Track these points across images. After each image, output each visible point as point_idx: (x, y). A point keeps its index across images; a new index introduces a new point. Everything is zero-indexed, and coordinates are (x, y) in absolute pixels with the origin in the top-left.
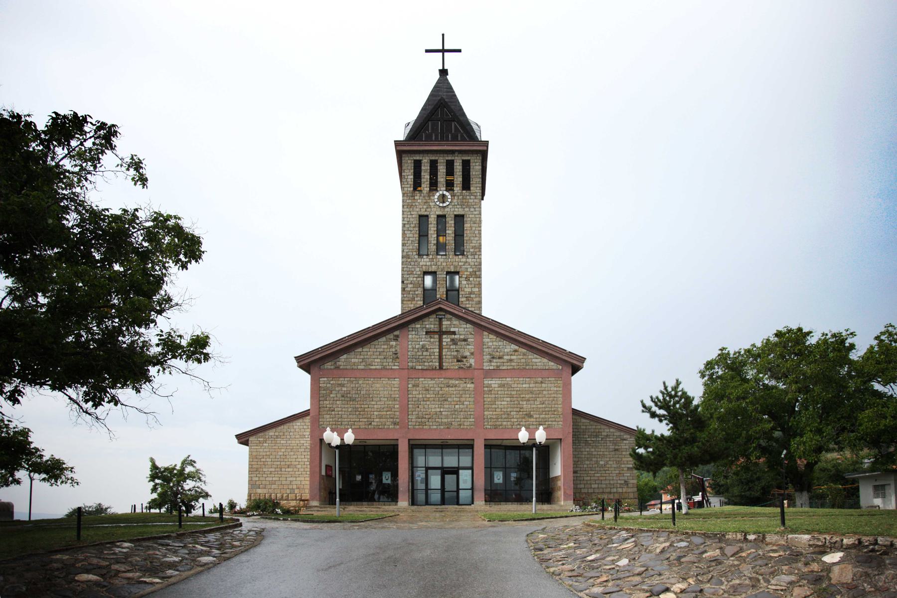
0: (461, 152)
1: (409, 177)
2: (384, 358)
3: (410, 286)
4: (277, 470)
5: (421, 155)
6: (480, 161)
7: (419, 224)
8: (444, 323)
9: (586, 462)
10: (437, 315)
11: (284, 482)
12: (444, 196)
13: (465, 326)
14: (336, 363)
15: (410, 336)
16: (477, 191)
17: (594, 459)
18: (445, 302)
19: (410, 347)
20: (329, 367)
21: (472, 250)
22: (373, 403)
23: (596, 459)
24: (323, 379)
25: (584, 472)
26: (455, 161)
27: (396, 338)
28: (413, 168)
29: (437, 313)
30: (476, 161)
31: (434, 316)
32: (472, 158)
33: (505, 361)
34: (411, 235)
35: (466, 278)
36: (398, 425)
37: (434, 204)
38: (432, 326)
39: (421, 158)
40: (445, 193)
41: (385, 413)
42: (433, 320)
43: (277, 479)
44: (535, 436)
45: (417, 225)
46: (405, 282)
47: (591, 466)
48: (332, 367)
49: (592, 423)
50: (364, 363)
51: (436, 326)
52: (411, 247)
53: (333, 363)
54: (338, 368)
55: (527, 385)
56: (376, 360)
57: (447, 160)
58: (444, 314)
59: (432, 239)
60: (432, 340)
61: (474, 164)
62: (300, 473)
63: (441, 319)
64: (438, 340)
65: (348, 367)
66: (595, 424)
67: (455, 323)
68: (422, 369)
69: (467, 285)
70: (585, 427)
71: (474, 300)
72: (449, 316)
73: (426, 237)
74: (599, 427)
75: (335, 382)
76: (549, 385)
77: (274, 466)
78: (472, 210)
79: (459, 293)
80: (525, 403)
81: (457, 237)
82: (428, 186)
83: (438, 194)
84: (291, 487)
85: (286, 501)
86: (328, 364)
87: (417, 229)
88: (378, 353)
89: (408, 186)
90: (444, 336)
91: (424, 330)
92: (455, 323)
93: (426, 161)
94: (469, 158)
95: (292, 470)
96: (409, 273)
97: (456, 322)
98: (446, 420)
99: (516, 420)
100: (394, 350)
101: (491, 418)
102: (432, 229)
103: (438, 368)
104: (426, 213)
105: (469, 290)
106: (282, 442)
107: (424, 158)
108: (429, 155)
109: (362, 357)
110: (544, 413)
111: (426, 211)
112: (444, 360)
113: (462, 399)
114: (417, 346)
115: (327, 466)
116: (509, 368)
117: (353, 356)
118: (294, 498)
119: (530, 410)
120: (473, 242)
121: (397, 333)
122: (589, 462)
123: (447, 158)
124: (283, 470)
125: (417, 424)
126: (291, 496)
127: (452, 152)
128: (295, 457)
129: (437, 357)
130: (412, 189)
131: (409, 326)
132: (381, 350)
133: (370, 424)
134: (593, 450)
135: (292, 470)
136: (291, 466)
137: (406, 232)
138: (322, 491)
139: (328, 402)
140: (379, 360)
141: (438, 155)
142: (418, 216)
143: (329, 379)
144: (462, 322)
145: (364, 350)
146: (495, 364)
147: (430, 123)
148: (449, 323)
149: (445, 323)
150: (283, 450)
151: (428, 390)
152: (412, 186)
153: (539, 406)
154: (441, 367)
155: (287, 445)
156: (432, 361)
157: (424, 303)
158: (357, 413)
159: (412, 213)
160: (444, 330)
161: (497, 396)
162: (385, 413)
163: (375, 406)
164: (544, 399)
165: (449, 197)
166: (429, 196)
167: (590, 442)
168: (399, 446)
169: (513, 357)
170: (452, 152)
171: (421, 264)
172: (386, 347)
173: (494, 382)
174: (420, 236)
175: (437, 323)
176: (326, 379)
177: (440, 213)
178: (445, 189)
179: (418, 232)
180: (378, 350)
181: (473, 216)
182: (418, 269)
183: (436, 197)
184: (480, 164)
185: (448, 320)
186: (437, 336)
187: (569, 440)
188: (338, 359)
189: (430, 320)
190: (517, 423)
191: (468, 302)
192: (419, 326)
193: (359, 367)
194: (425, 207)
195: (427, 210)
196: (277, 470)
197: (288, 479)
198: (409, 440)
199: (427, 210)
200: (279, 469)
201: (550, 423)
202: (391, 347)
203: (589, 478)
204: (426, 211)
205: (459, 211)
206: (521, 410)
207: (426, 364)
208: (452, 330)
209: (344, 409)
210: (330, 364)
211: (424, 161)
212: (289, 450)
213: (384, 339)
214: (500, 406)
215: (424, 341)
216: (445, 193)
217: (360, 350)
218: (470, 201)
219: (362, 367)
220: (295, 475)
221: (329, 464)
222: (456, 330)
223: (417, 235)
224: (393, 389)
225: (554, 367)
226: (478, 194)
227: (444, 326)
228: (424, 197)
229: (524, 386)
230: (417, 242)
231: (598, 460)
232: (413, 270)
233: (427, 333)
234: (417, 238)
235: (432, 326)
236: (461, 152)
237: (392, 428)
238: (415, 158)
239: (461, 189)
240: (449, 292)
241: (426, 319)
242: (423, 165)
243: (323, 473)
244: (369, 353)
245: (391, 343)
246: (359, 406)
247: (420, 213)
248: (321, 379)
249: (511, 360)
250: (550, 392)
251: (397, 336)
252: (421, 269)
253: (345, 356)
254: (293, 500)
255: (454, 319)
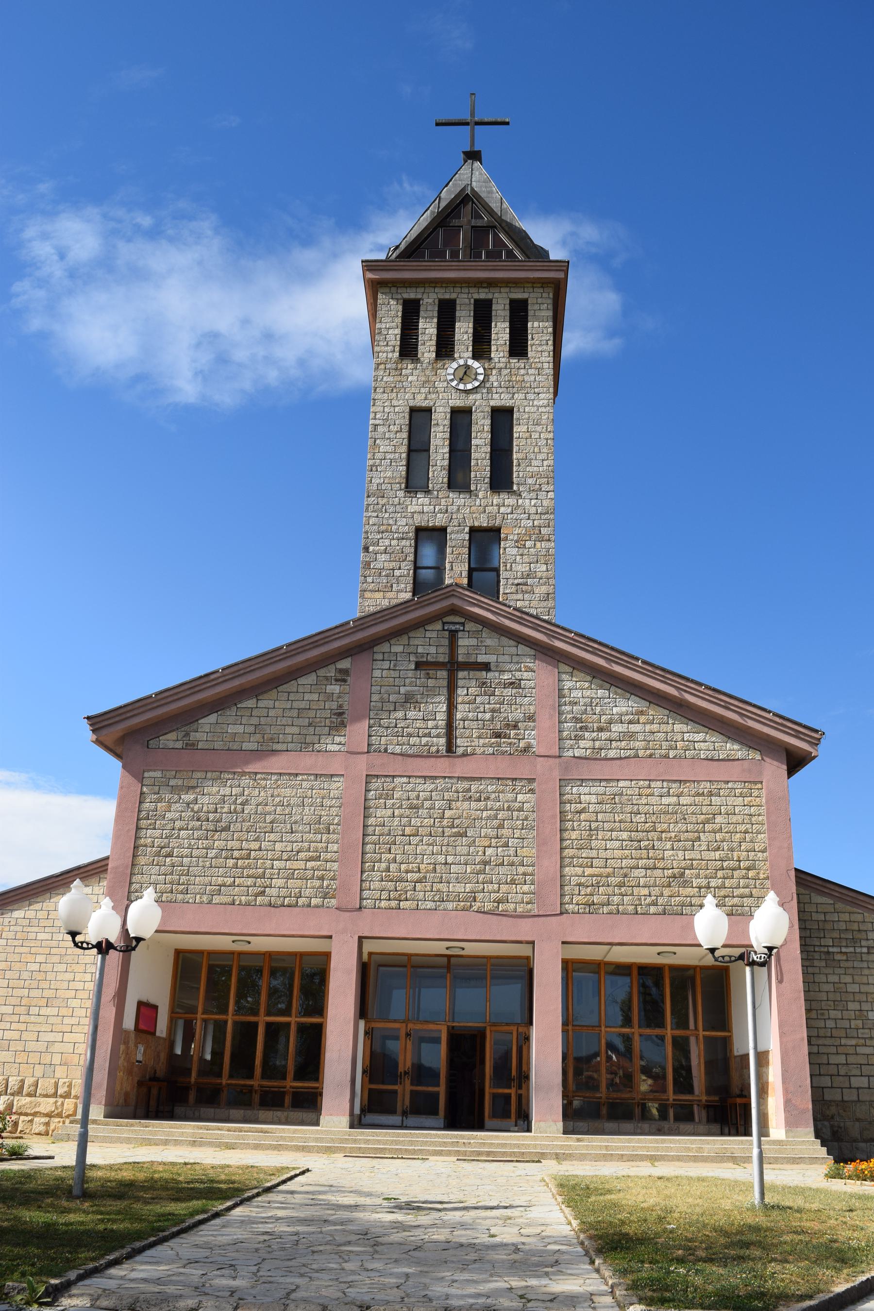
0: (434, 283)
1: (391, 332)
2: (310, 725)
3: (384, 557)
4: (18, 1010)
5: (421, 290)
6: (550, 301)
7: (410, 425)
8: (461, 642)
9: (833, 1014)
10: (444, 623)
11: (31, 1046)
12: (467, 367)
13: (513, 650)
14: (187, 734)
15: (377, 673)
16: (543, 359)
17: (851, 1006)
18: (467, 593)
19: (375, 697)
20: (171, 745)
21: (530, 481)
22: (272, 837)
23: (856, 1006)
24: (152, 774)
25: (828, 1041)
26: (494, 301)
27: (343, 677)
28: (400, 314)
29: (445, 620)
30: (540, 301)
31: (438, 626)
32: (532, 295)
33: (614, 736)
34: (389, 449)
35: (517, 541)
36: (333, 897)
37: (445, 384)
38: (433, 650)
39: (419, 296)
40: (470, 362)
41: (301, 864)
42: (434, 635)
43: (15, 1035)
44: (696, 938)
45: (406, 428)
46: (371, 549)
47: (846, 1024)
48: (179, 745)
49: (840, 906)
50: (258, 737)
51: (441, 650)
52: (389, 474)
53: (181, 735)
54: (191, 746)
55: (674, 800)
56: (288, 730)
57: (476, 300)
58: (463, 620)
59: (440, 457)
60: (431, 683)
61: (536, 307)
62: (74, 1021)
63: (453, 636)
64: (445, 683)
65: (217, 745)
66: (849, 908)
67: (489, 642)
68: (401, 755)
69: (518, 557)
70: (822, 917)
71: (537, 590)
72: (470, 626)
73: (425, 453)
74: (859, 918)
75: (180, 782)
76: (731, 800)
77: (13, 1001)
78: (531, 396)
79: (498, 575)
80: (668, 845)
81: (413, 454)
82: (433, 348)
83: (455, 365)
84: (46, 1059)
85: (28, 1099)
86: (169, 736)
87: (405, 435)
88: (295, 713)
89: (389, 348)
90: (461, 674)
91: (413, 658)
92: (489, 642)
93: (430, 301)
94: (525, 296)
95: (54, 1011)
96: (382, 528)
97: (491, 641)
98: (459, 888)
99: (645, 891)
100: (334, 705)
101: (579, 885)
102: (439, 435)
103: (443, 749)
104: (425, 404)
105: (525, 568)
106: (41, 936)
107: (425, 296)
108: (437, 290)
109: (255, 721)
110: (720, 874)
111: (426, 399)
112: (458, 732)
113: (505, 832)
114: (393, 698)
115: (141, 1005)
116: (623, 753)
117: (231, 720)
118: (51, 1091)
119: (683, 864)
120: (534, 463)
121: (344, 664)
122: (838, 1014)
123: (476, 296)
124: (34, 1010)
125: (385, 895)
126: (46, 1085)
127: (491, 284)
128: (70, 976)
129: (442, 724)
130: (434, 355)
131: (376, 649)
132: (303, 705)
133: (262, 893)
134: (848, 979)
135: (54, 1011)
136: (56, 1002)
137: (378, 441)
138: (120, 1074)
139: (157, 833)
140: (295, 730)
141: (458, 290)
142: (408, 410)
143: (168, 774)
144: (505, 641)
145: (261, 704)
146: (589, 744)
147: (441, 232)
148: (473, 642)
149: (464, 642)
150: (40, 958)
151: (416, 807)
152: (397, 349)
153: (706, 855)
154: (450, 747)
155: (54, 943)
156: (429, 735)
157: (414, 595)
158: (231, 862)
159: (395, 403)
160: (461, 659)
161: (594, 825)
162: (301, 864)
163: (278, 846)
164: (719, 836)
165: (481, 370)
166: (435, 370)
167: (838, 957)
168: (332, 955)
169: (633, 728)
170: (491, 284)
171: (410, 509)
172: (315, 697)
173: (586, 790)
174: (410, 451)
175: (446, 642)
176: (158, 774)
177: (459, 403)
178: (470, 354)
179: (406, 442)
180: (296, 705)
181: (533, 409)
182: (403, 522)
183: (451, 371)
184: (551, 307)
185: (471, 634)
186: (443, 674)
187: (794, 955)
188: (195, 726)
189: (428, 634)
190: (649, 900)
191: (520, 596)
192: (399, 649)
193: (245, 746)
194: (423, 390)
195: (429, 396)
196: (18, 1010)
197: (43, 1037)
198: (361, 939)
199: (429, 396)
200: (22, 1010)
201: (736, 900)
202: (330, 697)
203: (842, 1059)
204: (426, 399)
205: (500, 400)
206: (661, 864)
207: (413, 740)
208: (481, 659)
209: (195, 853)
210: (172, 736)
211: (426, 301)
212: (56, 959)
213: (311, 679)
214: (602, 854)
215: (410, 685)
216: (470, 362)
217: (251, 703)
218: (526, 378)
219: (253, 746)
220: (59, 1028)
221: (153, 1001)
222: (491, 659)
223: (404, 449)
224: (328, 803)
225: (739, 755)
226: (546, 365)
227: (461, 651)
228: (423, 370)
229: (665, 800)
230: (404, 463)
231: (865, 1007)
232: (391, 522)
233: (419, 666)
234: (404, 455)
235: (433, 650)
236: (434, 283)
237: (317, 906)
238: (406, 296)
239: (507, 354)
240: (475, 574)
241: (419, 633)
242: (422, 308)
243: (129, 1023)
244: (272, 713)
245: (330, 689)
246: (235, 844)
247: (412, 403)
248: (146, 775)
249: (631, 736)
250: (734, 819)
251: (346, 672)
252: (411, 521)
253: (213, 718)
254: (46, 1096)
255: (486, 633)
